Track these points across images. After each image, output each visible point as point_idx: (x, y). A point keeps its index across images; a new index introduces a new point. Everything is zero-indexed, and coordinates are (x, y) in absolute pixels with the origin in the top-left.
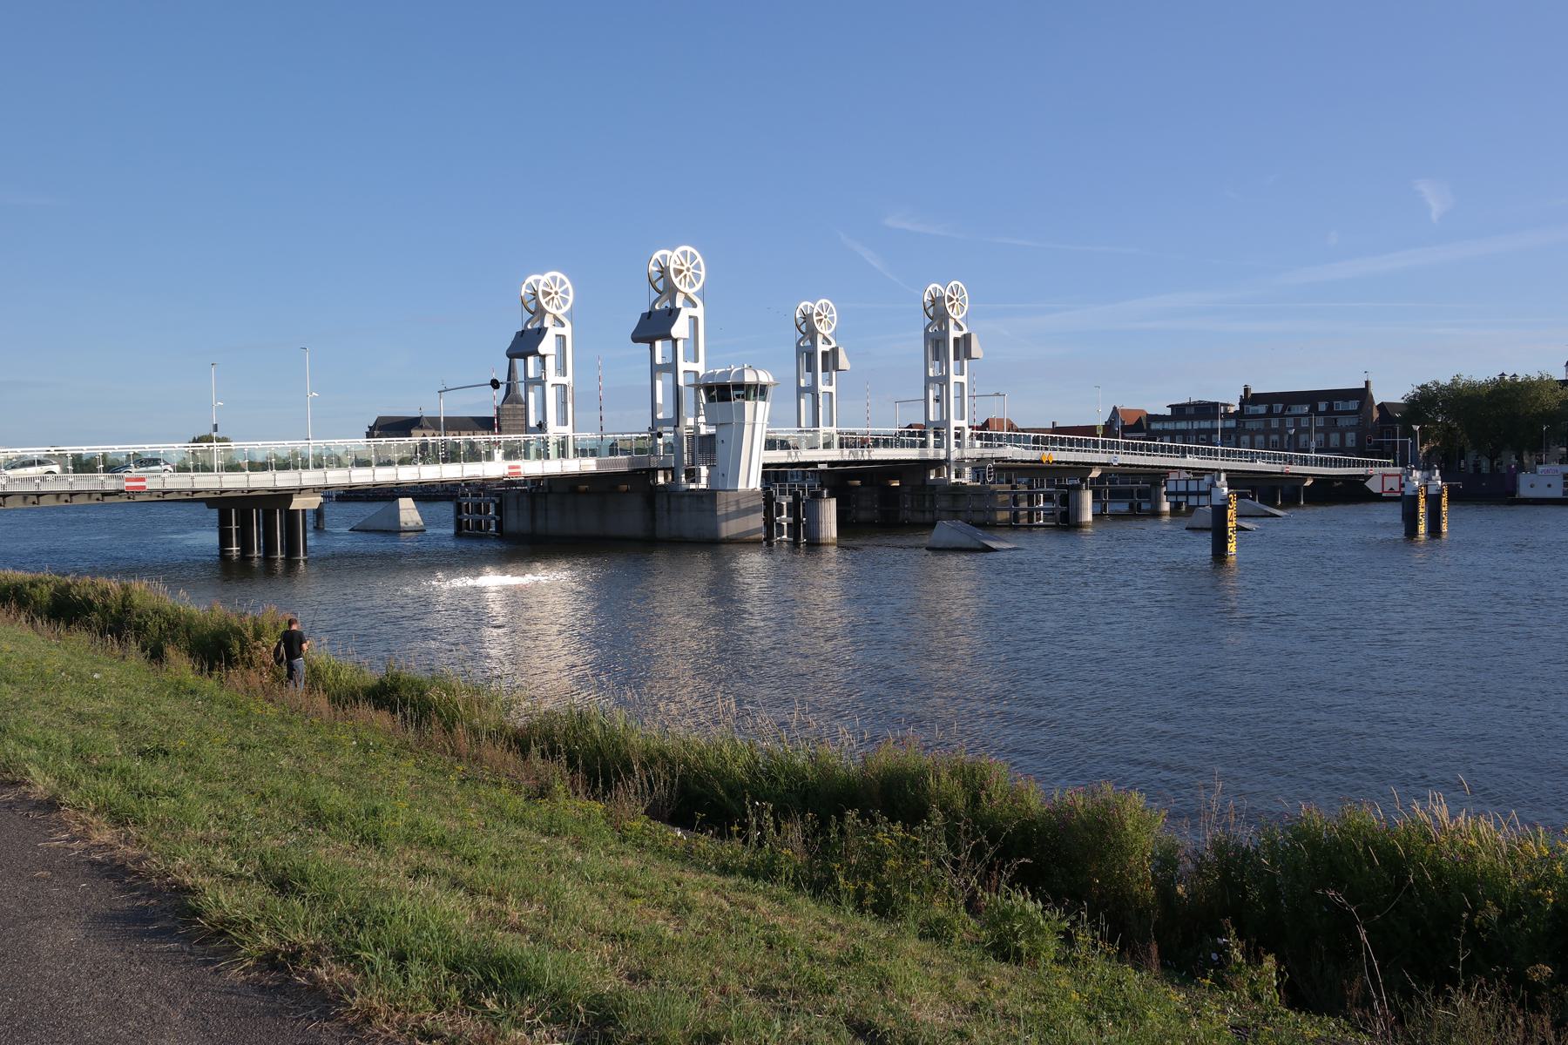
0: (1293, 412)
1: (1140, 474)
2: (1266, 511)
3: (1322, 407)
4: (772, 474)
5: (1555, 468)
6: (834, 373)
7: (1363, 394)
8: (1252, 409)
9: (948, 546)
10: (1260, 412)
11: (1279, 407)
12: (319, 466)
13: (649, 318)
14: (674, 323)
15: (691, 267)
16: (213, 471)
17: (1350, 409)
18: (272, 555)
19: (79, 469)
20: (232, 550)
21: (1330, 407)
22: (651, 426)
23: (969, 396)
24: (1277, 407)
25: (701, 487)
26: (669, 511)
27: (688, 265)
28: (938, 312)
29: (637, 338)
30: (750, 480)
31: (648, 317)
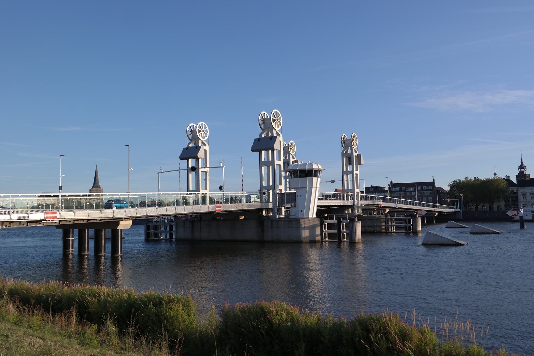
0: (408, 190)
1: (396, 212)
2: (461, 225)
3: (419, 188)
4: (321, 211)
5: (529, 209)
6: (358, 165)
7: (432, 184)
8: (394, 189)
9: (434, 243)
10: (397, 190)
11: (403, 188)
12: (133, 206)
13: (187, 150)
14: (275, 143)
15: (204, 130)
16: (61, 195)
17: (429, 189)
18: (100, 253)
19: (97, 208)
20: (70, 251)
21: (422, 188)
22: (260, 189)
23: (350, 180)
24: (425, 188)
25: (281, 216)
26: (272, 227)
27: (203, 129)
28: (347, 144)
29: (254, 150)
30: (312, 214)
31: (186, 150)
